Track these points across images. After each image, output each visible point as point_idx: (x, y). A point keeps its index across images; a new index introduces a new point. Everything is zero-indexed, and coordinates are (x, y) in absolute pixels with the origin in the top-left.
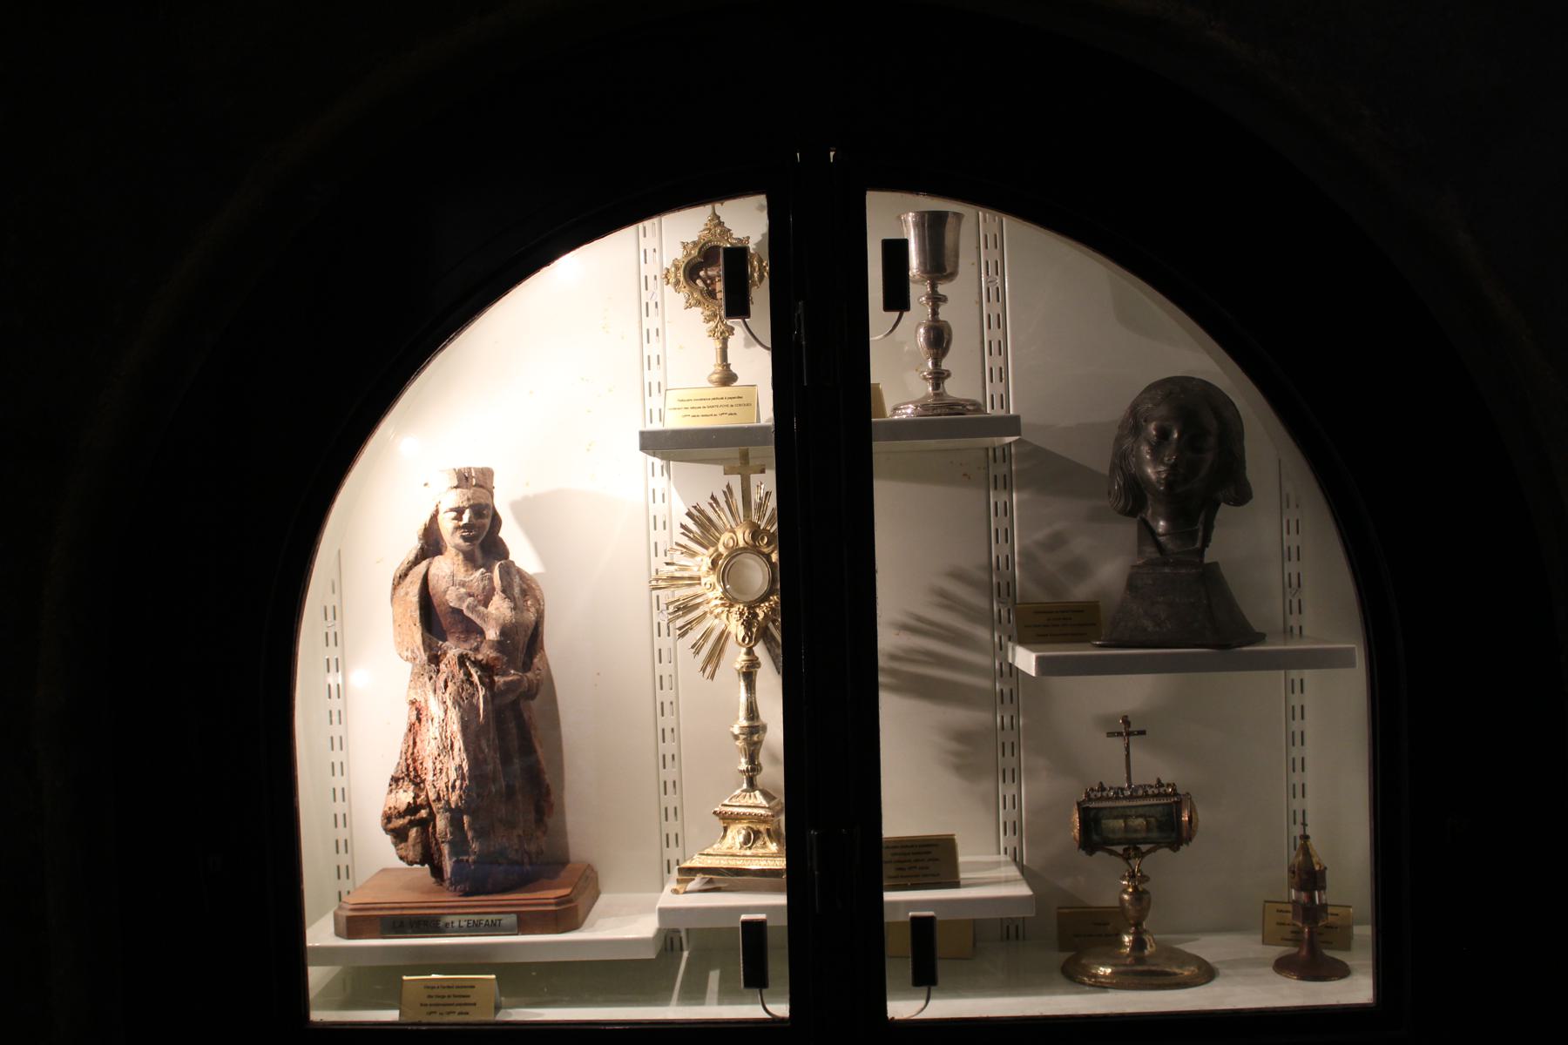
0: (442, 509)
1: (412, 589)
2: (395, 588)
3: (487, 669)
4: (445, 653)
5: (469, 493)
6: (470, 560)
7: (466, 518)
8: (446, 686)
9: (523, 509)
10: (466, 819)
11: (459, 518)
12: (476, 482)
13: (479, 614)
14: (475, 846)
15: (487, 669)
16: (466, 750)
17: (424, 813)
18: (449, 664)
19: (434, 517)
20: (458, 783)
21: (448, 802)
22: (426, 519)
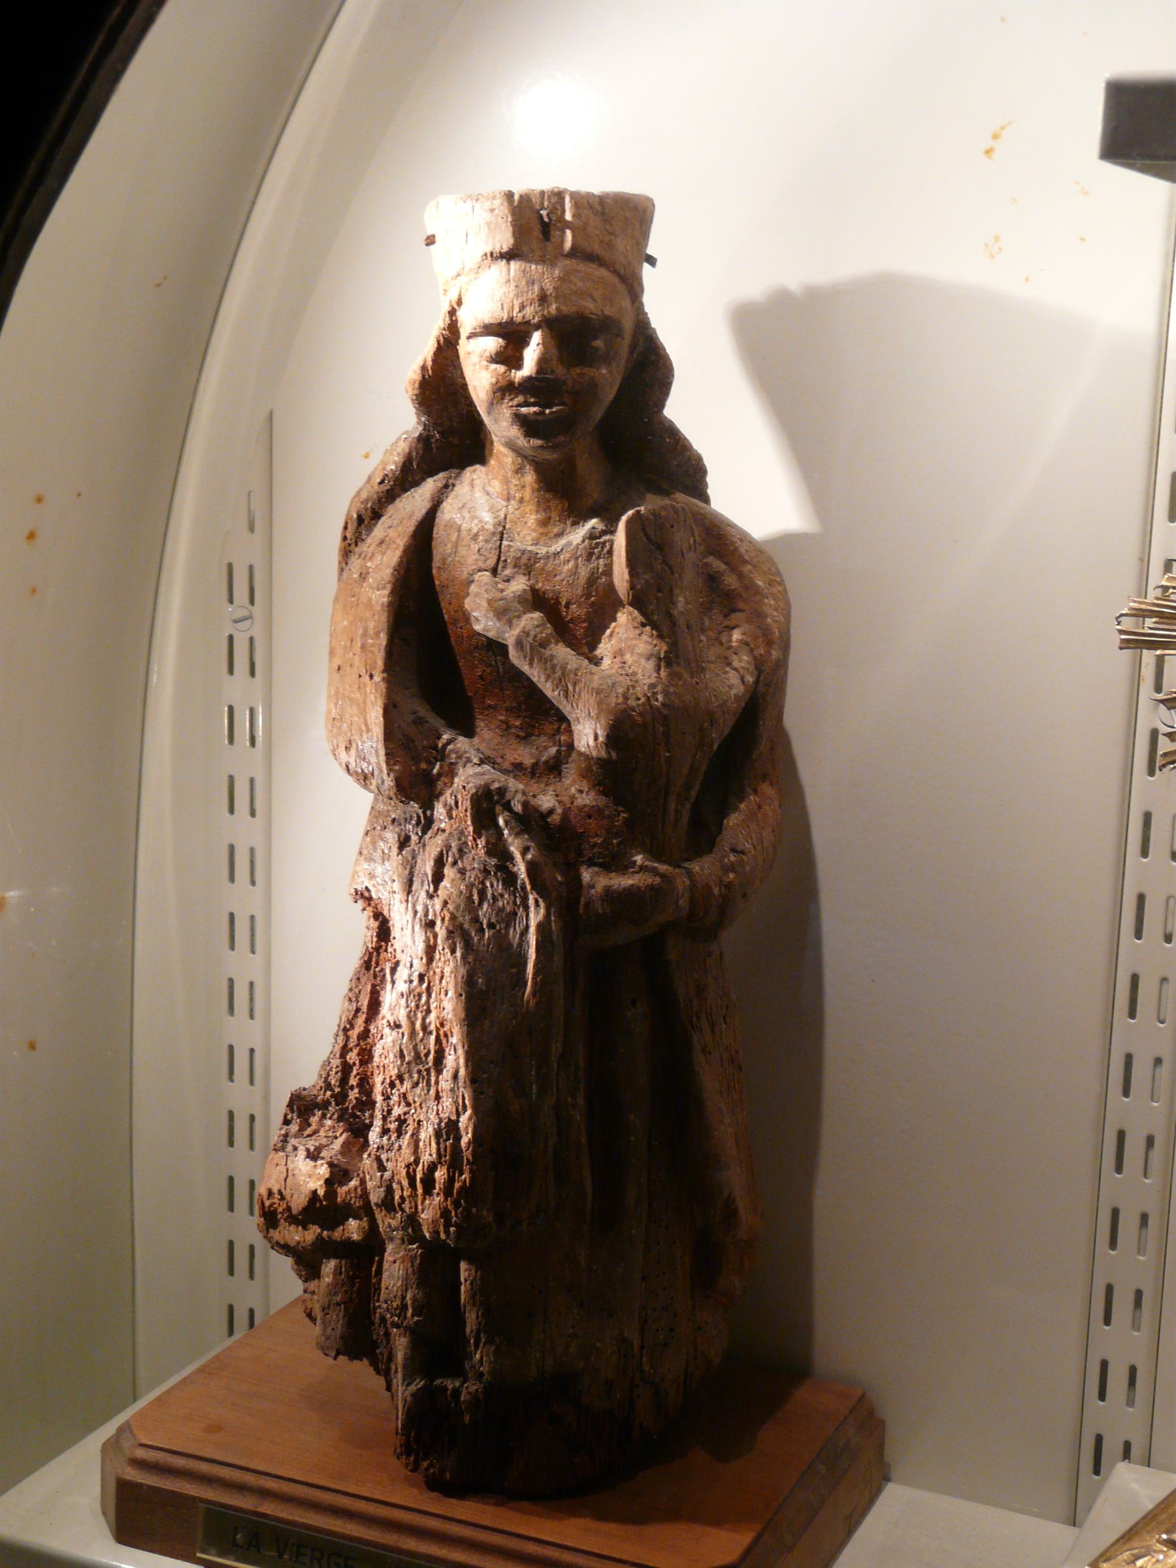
0: (468, 321)
1: (383, 556)
2: (346, 553)
3: (556, 839)
4: (451, 773)
5: (547, 277)
6: (562, 491)
7: (531, 355)
8: (438, 878)
9: (784, 341)
10: (465, 1270)
11: (509, 357)
12: (582, 253)
13: (550, 667)
14: (481, 1357)
15: (556, 839)
16: (474, 1080)
17: (353, 1228)
18: (451, 813)
19: (448, 346)
20: (440, 1174)
21: (412, 1220)
22: (426, 350)
